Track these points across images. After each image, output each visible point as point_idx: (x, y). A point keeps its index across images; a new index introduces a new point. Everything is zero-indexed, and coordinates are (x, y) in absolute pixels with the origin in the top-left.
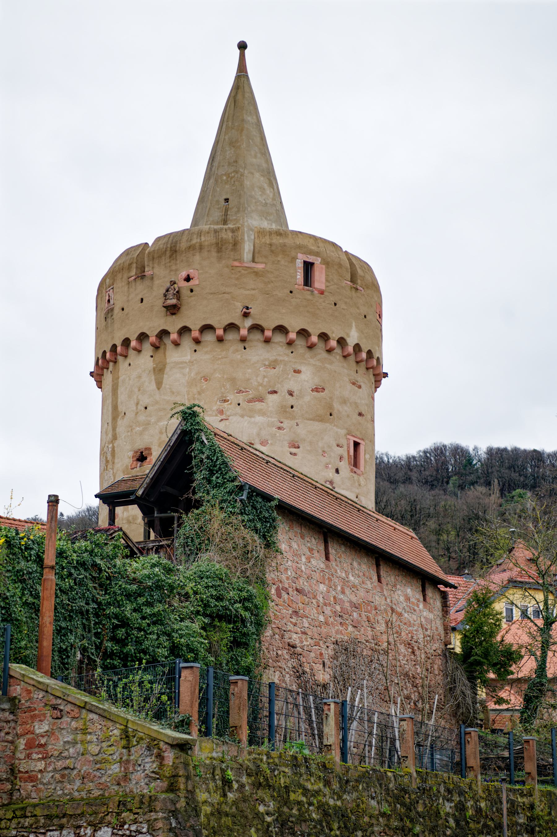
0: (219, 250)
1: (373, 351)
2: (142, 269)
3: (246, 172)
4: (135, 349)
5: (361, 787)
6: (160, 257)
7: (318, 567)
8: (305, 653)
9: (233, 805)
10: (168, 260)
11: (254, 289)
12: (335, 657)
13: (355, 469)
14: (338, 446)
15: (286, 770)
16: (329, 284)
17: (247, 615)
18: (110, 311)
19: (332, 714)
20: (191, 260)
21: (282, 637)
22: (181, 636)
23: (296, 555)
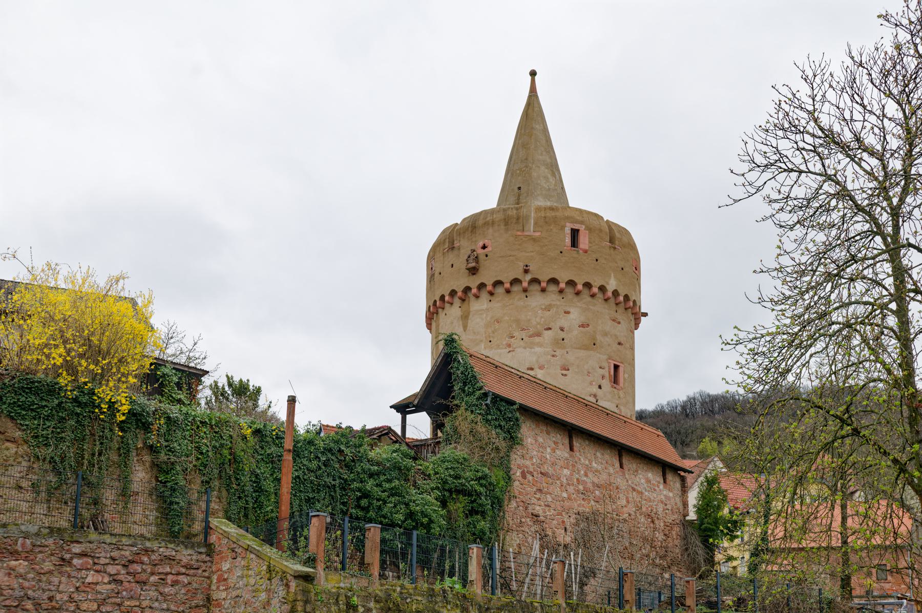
0: (506, 224)
2: (452, 242)
4: (448, 302)
8: (547, 521)
15: (420, 598)
17: (482, 490)
18: (433, 275)
19: (474, 556)
21: (526, 508)
23: (542, 447)
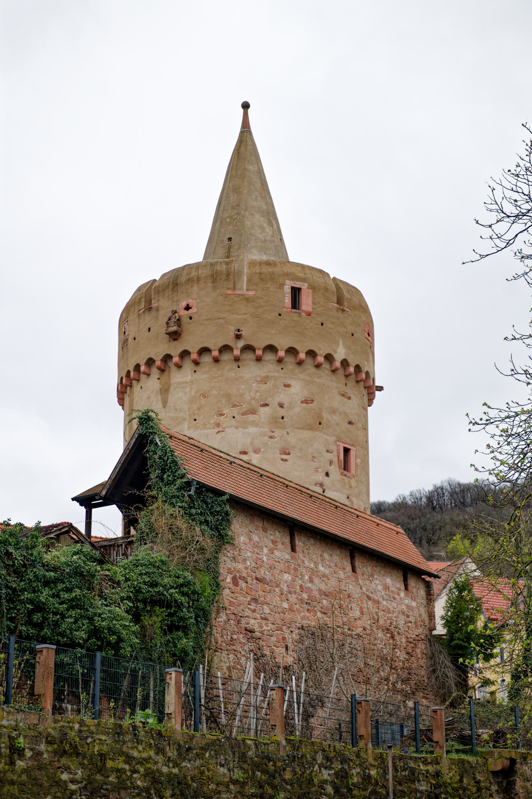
0: (214, 281)
1: (361, 365)
2: (149, 302)
3: (247, 213)
4: (145, 373)
5: (207, 755)
6: (164, 290)
7: (282, 558)
9: (22, 773)
10: (171, 293)
11: (245, 314)
12: (301, 641)
13: (345, 472)
14: (327, 451)
15: (104, 738)
16: (315, 307)
20: (190, 292)
21: (239, 622)
22: (104, 620)
